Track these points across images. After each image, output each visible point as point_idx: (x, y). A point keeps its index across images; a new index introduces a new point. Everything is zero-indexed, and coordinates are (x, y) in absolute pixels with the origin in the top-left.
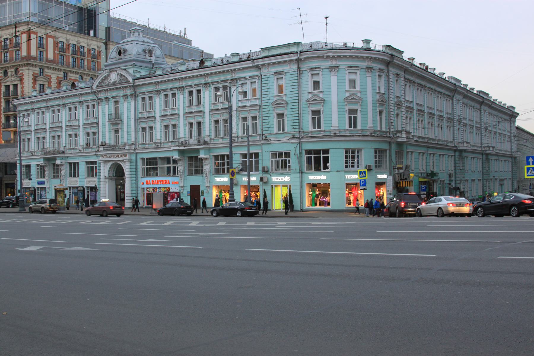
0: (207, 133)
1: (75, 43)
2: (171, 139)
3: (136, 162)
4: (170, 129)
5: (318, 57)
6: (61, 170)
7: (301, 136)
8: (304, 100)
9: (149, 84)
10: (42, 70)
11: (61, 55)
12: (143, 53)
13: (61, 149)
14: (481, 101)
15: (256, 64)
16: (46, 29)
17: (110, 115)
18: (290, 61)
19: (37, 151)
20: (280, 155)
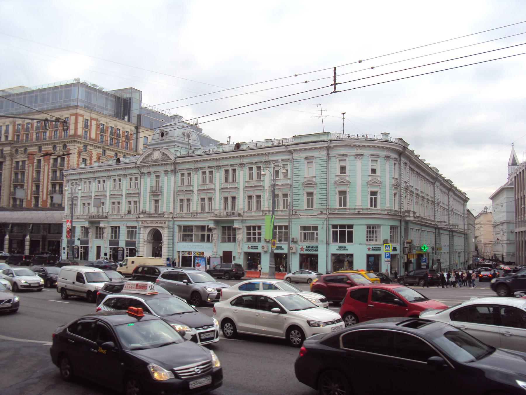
0: (241, 207)
1: (113, 126)
2: (207, 210)
3: (174, 228)
4: (207, 202)
5: (346, 146)
6: (103, 232)
7: (330, 213)
8: (333, 182)
9: (189, 162)
10: (85, 146)
11: (102, 135)
12: (182, 136)
13: (105, 214)
14: (449, 188)
15: (289, 149)
16: (91, 113)
17: (151, 187)
18: (320, 148)
19: (82, 215)
20: (309, 228)
